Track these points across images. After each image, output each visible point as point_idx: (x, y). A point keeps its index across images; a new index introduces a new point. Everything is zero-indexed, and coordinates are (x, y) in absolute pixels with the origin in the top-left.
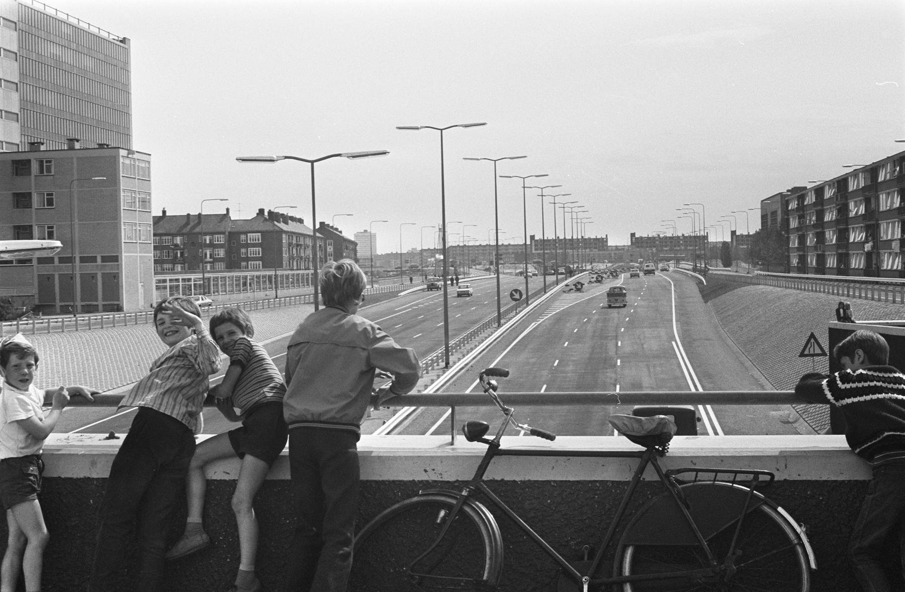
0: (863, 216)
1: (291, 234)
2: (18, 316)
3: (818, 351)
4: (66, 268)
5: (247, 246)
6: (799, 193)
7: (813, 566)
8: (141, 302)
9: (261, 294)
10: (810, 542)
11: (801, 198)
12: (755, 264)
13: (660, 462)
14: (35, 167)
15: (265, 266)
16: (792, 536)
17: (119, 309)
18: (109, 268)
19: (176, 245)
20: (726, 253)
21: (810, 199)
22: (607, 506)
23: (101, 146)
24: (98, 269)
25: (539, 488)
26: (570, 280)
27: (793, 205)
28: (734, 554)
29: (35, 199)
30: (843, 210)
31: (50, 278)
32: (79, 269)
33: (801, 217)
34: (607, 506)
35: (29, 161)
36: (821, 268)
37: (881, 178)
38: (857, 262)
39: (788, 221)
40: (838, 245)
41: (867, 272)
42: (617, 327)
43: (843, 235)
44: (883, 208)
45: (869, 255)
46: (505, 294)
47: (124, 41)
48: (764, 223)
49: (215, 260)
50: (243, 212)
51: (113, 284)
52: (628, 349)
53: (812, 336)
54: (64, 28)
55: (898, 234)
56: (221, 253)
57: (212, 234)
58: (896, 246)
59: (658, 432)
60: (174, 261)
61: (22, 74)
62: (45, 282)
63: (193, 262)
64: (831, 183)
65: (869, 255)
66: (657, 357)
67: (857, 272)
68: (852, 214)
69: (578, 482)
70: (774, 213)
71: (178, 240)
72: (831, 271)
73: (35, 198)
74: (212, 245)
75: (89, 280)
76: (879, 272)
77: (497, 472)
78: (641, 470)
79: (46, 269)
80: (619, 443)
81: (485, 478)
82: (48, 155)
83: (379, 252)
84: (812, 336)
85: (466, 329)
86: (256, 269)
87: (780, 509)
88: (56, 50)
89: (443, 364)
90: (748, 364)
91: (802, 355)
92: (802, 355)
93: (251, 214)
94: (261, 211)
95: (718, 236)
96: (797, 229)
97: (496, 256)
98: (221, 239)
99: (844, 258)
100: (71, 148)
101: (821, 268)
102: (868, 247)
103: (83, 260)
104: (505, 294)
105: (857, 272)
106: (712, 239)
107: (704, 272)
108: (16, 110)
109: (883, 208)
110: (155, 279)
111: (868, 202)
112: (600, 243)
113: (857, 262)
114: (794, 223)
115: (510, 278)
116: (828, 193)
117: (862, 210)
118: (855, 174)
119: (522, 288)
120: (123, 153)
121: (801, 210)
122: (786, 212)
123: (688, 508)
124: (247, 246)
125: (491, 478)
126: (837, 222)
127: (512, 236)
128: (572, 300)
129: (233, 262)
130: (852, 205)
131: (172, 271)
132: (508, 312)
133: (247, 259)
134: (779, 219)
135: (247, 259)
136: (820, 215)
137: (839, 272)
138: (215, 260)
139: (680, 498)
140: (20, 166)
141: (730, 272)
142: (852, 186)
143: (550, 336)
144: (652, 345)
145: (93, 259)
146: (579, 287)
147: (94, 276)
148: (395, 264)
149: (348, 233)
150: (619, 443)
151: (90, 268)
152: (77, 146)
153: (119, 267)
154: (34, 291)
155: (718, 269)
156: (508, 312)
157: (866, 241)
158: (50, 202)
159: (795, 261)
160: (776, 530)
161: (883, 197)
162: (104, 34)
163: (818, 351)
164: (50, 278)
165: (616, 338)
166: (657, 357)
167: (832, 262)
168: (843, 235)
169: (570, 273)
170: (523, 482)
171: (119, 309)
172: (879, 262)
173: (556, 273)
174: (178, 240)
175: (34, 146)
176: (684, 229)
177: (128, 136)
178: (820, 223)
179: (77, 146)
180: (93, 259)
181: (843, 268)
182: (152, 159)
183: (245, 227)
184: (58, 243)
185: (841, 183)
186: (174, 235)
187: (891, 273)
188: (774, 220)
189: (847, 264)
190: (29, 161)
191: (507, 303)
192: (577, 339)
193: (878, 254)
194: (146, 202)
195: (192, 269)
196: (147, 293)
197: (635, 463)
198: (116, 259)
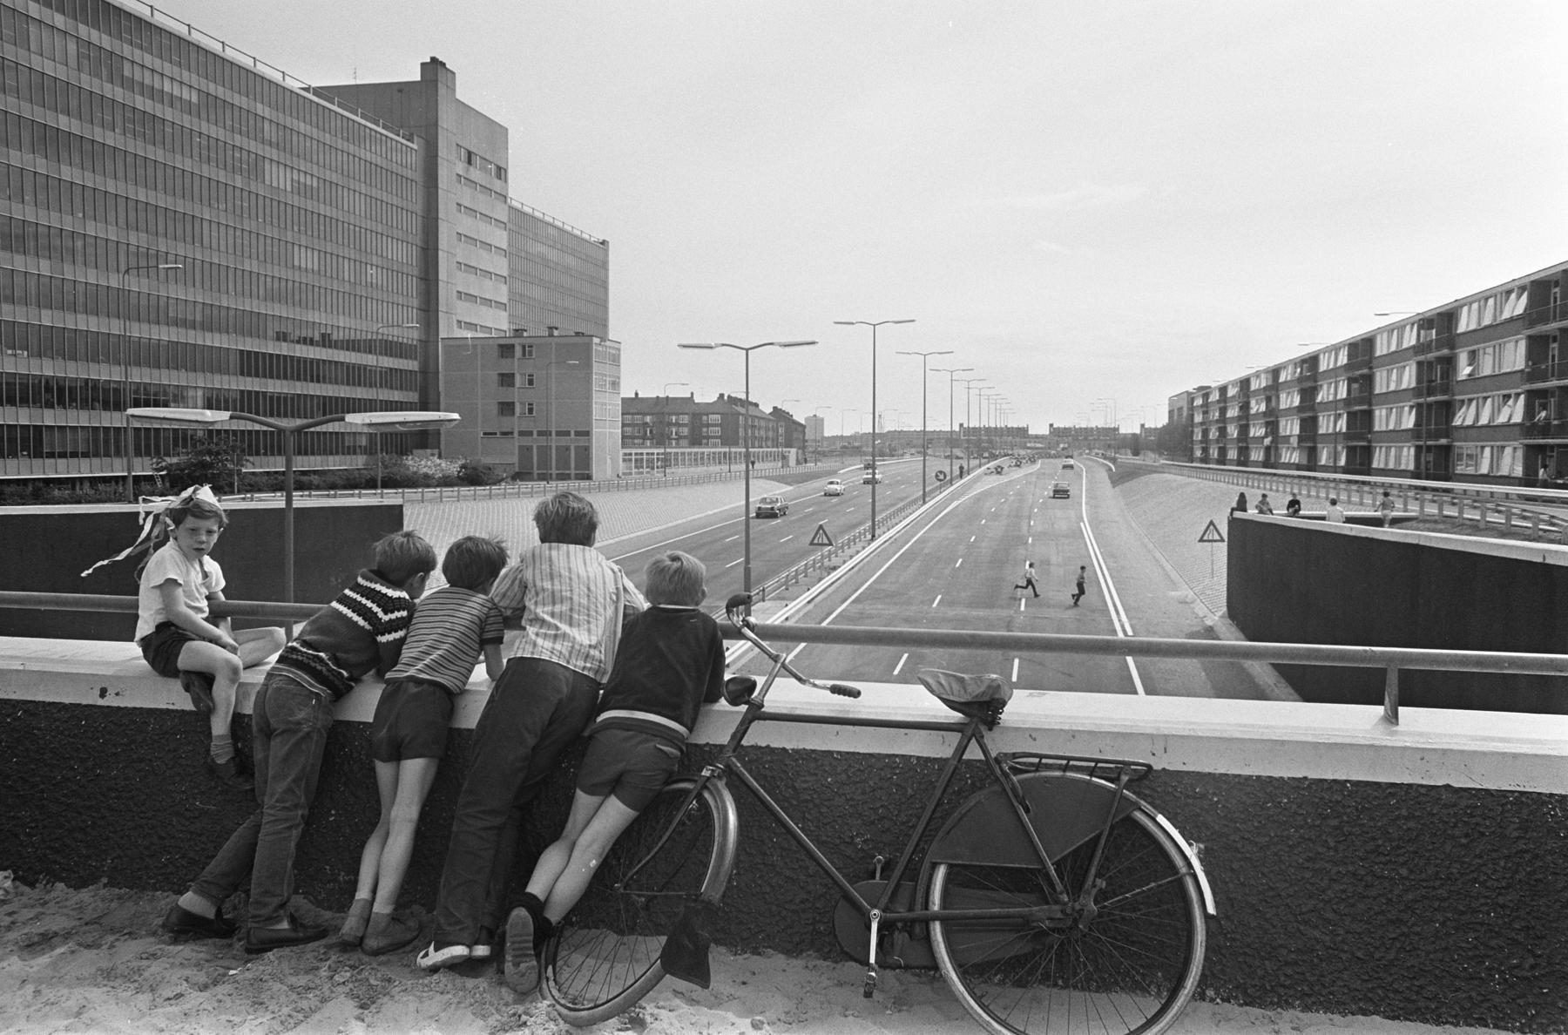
0: (1264, 414)
1: (746, 416)
2: (498, 482)
3: (1217, 537)
4: (542, 441)
5: (708, 425)
6: (1205, 391)
7: (1211, 910)
8: (609, 471)
9: (717, 468)
10: (1207, 874)
11: (1206, 396)
12: (1161, 454)
13: (989, 738)
14: (518, 351)
15: (723, 444)
16: (1179, 862)
17: (589, 477)
18: (582, 441)
19: (646, 424)
20: (1135, 444)
21: (1215, 397)
22: (910, 791)
23: (577, 334)
24: (572, 442)
25: (816, 760)
26: (992, 464)
27: (1199, 402)
28: (1094, 886)
29: (518, 380)
30: (1245, 407)
31: (529, 449)
32: (554, 442)
33: (1205, 413)
34: (910, 791)
35: (513, 346)
36: (1222, 460)
37: (1282, 379)
38: (1257, 455)
39: (1192, 416)
40: (1239, 440)
41: (1266, 464)
42: (1031, 508)
43: (1244, 430)
44: (1282, 406)
45: (1268, 449)
46: (931, 474)
47: (603, 243)
48: (1171, 416)
49: (679, 438)
50: (706, 396)
51: (585, 456)
52: (1039, 529)
53: (1211, 523)
54: (551, 231)
55: (1296, 431)
56: (685, 431)
57: (678, 414)
58: (1294, 441)
59: (986, 698)
60: (644, 438)
61: (512, 270)
62: (525, 451)
63: (661, 439)
64: (1234, 383)
65: (1268, 449)
66: (1067, 536)
67: (1256, 464)
68: (1253, 411)
69: (871, 755)
70: (1180, 409)
71: (648, 419)
72: (1231, 462)
73: (518, 378)
74: (677, 424)
75: (544, 452)
76: (1368, 471)
77: (758, 736)
78: (962, 749)
79: (526, 441)
80: (932, 707)
81: (744, 743)
82: (529, 341)
83: (826, 434)
84: (1211, 523)
85: (893, 505)
86: (715, 446)
87: (1161, 819)
88: (540, 248)
89: (869, 537)
90: (1151, 546)
91: (1201, 540)
92: (1201, 540)
93: (713, 398)
94: (722, 396)
95: (1130, 428)
96: (1202, 424)
97: (924, 442)
98: (685, 419)
99: (1244, 451)
100: (551, 335)
101: (1222, 460)
102: (1267, 441)
103: (559, 433)
104: (931, 474)
105: (1256, 464)
106: (1122, 431)
107: (1114, 460)
108: (504, 300)
109: (1282, 406)
110: (622, 452)
111: (1268, 400)
112: (1022, 432)
113: (1257, 455)
114: (1198, 418)
115: (937, 464)
116: (1231, 392)
117: (1263, 408)
118: (1257, 375)
119: (947, 470)
120: (596, 340)
121: (1206, 408)
122: (1192, 408)
123: (1027, 811)
124: (708, 425)
125: (752, 743)
126: (1239, 418)
127: (940, 423)
128: (994, 481)
129: (696, 440)
130: (1253, 403)
131: (642, 445)
132: (932, 491)
133: (708, 438)
134: (1185, 413)
135: (708, 438)
136: (1223, 411)
137: (1239, 463)
138: (679, 438)
139: (1016, 796)
140: (506, 350)
141: (1138, 460)
142: (1254, 386)
143: (971, 514)
144: (1062, 526)
145: (568, 433)
146: (999, 471)
147: (568, 449)
148: (839, 445)
149: (800, 418)
150: (932, 707)
151: (564, 441)
152: (556, 333)
153: (590, 441)
154: (515, 459)
155: (1126, 458)
156: (932, 491)
157: (1266, 436)
158: (531, 382)
159: (1198, 453)
160: (1157, 856)
161: (1283, 396)
162: (586, 236)
163: (1217, 537)
164: (529, 449)
165: (1030, 518)
166: (1067, 536)
167: (1232, 454)
168: (1244, 430)
169: (994, 457)
170: (796, 751)
171: (589, 477)
172: (1278, 456)
173: (981, 456)
174: (648, 419)
175: (518, 332)
176: (1097, 422)
177: (605, 326)
178: (1223, 419)
179: (556, 333)
180: (568, 433)
181: (1243, 460)
182: (622, 347)
183: (708, 409)
184: (456, 416)
185: (1245, 383)
186: (645, 414)
187: (1288, 466)
188: (1180, 415)
189: (1247, 456)
190: (513, 346)
191: (932, 484)
192: (995, 517)
193: (1277, 449)
194: (615, 384)
195: (660, 444)
196: (615, 467)
197: (954, 738)
198: (587, 434)
